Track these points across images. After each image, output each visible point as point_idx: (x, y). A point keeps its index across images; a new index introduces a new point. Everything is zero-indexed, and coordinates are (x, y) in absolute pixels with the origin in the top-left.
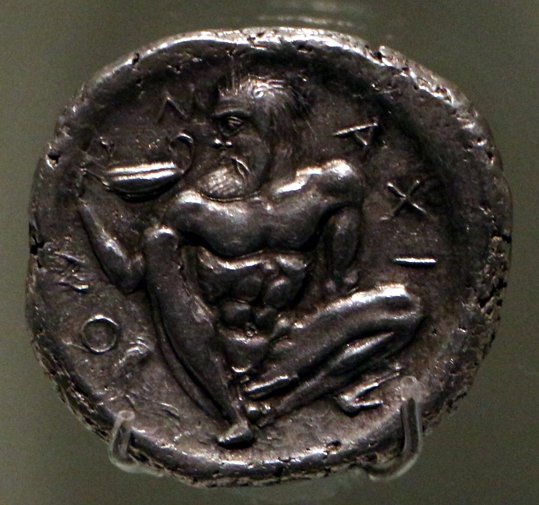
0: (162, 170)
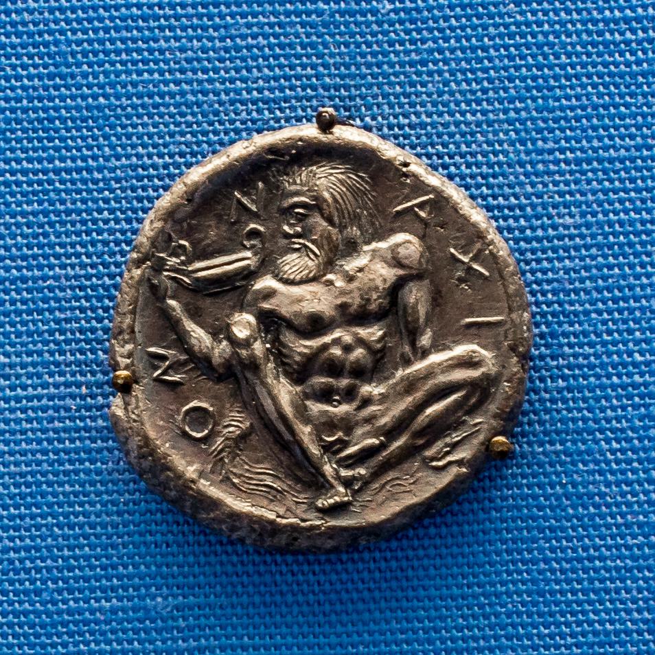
0: (246, 258)
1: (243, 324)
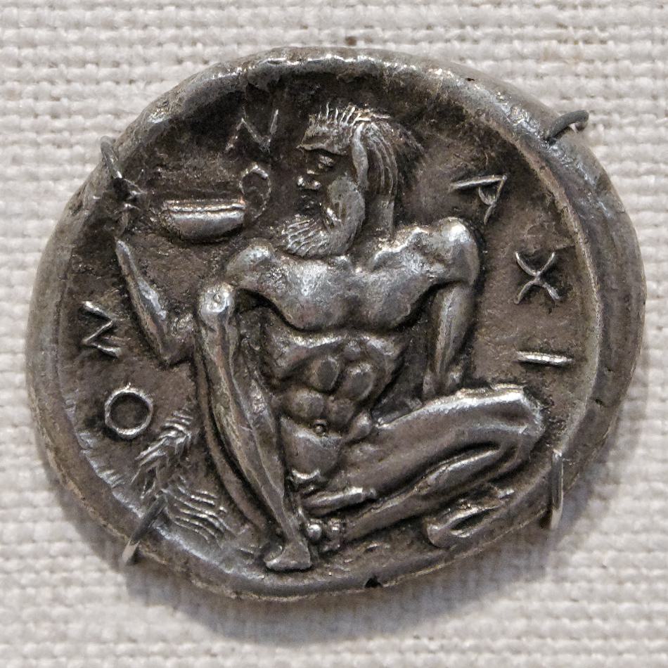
1: (218, 301)
